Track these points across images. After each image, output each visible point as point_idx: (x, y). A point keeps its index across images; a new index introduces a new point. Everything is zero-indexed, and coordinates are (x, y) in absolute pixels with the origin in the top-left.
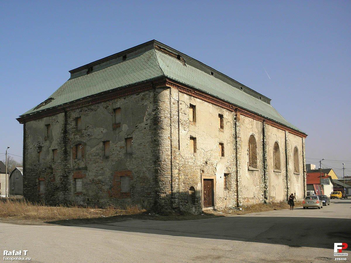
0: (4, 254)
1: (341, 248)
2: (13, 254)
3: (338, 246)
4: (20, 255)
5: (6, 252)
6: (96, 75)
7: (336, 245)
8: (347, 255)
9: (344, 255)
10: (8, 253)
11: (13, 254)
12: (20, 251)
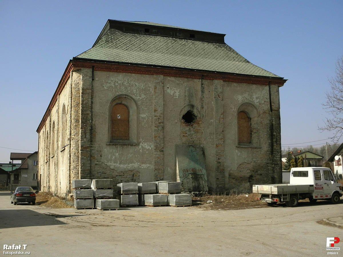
0: (4, 249)
1: (333, 242)
2: (13, 249)
3: (331, 241)
4: (20, 249)
5: (6, 246)
7: (328, 239)
8: (339, 249)
10: (7, 247)
11: (13, 249)
12: (20, 245)
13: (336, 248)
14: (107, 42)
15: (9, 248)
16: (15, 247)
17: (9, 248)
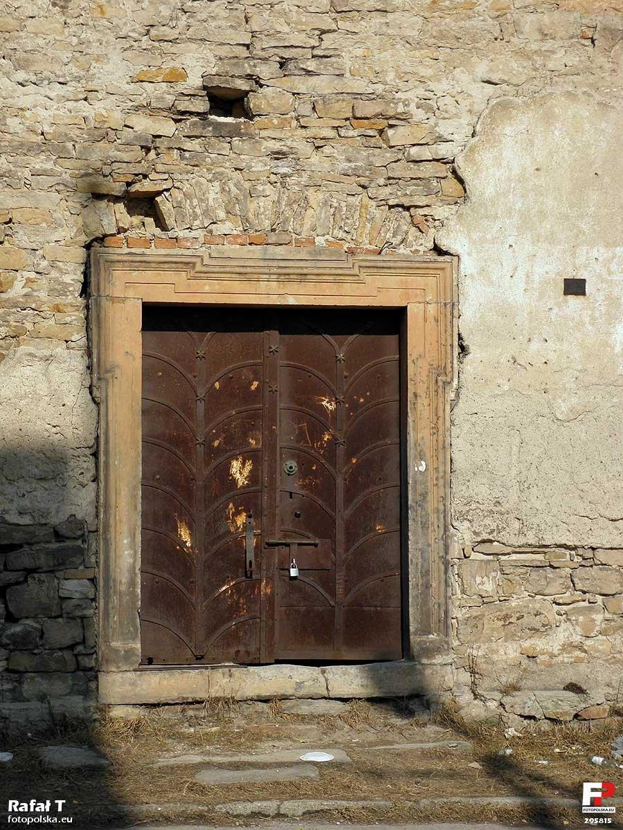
0: (10, 810)
1: (598, 794)
2: (32, 810)
3: (593, 790)
4: (48, 810)
5: (14, 804)
6: (418, 270)
8: (614, 812)
9: (606, 812)
10: (18, 807)
11: (32, 810)
12: (48, 802)
13: (605, 808)
14: (62, 728)
15: (21, 809)
16: (35, 807)
17: (37, 809)
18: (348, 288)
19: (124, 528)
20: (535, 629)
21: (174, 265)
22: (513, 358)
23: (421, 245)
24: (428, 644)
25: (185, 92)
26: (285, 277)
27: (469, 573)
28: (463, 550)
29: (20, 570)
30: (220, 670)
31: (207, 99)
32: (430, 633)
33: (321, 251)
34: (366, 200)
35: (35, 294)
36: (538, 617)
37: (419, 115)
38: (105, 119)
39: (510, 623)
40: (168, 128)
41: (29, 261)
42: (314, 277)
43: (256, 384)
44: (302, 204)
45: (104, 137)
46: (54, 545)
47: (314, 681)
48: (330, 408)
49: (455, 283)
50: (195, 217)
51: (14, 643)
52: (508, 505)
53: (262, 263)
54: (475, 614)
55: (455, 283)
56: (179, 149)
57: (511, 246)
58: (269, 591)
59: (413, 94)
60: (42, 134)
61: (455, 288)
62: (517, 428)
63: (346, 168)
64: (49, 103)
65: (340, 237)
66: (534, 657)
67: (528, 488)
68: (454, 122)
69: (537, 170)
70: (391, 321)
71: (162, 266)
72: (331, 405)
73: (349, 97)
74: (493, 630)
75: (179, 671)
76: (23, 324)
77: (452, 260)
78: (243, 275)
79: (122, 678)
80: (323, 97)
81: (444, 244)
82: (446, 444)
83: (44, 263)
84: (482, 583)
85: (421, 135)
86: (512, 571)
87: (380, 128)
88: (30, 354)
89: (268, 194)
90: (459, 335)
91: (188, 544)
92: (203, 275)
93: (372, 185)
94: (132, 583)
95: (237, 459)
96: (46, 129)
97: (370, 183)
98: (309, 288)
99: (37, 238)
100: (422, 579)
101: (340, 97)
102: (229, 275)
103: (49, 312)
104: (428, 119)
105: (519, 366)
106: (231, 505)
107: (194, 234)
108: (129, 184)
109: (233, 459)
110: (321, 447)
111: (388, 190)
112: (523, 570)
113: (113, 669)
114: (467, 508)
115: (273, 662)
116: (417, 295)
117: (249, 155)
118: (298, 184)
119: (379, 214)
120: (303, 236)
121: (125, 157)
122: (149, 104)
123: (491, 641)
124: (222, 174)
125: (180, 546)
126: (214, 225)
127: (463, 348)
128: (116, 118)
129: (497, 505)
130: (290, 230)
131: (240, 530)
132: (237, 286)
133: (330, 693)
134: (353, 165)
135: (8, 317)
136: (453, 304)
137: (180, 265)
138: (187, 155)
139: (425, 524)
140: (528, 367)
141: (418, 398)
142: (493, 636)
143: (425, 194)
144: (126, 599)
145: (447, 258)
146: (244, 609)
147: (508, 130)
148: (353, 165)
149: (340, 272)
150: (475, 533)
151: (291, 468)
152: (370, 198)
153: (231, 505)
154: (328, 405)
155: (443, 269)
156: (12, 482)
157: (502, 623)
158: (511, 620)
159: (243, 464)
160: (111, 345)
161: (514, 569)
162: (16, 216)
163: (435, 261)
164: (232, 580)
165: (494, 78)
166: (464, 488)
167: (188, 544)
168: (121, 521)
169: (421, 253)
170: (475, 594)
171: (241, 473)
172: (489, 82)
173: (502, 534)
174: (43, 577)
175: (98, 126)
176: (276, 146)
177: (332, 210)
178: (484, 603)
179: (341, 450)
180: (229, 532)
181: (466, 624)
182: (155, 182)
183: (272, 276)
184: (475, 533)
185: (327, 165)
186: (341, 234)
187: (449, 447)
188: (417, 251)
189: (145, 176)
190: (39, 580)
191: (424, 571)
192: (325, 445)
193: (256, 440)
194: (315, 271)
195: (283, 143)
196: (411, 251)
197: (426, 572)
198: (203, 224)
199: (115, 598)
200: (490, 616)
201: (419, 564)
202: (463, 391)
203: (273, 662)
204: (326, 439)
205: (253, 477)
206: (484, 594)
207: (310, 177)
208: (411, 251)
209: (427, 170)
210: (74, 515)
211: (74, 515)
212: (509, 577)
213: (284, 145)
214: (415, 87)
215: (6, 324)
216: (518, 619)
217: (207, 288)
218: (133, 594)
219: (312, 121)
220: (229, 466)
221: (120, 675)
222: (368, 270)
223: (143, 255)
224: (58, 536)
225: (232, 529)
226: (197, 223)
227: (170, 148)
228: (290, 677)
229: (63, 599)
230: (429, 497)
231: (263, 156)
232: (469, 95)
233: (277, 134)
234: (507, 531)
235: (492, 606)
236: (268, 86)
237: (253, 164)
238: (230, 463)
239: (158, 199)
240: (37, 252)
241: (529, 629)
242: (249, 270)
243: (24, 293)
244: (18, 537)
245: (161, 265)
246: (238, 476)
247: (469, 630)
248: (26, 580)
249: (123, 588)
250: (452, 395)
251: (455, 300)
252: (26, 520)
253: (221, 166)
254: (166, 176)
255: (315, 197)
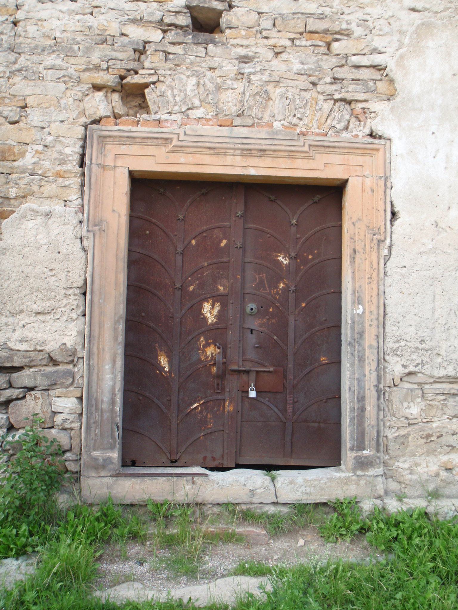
18: (299, 163)
19: (107, 356)
20: (452, 446)
21: (155, 141)
22: (436, 222)
23: (360, 131)
24: (363, 459)
25: (171, 9)
26: (247, 153)
27: (398, 399)
28: (393, 380)
29: (21, 388)
30: (185, 478)
31: (189, 15)
32: (364, 449)
33: (277, 132)
34: (315, 95)
35: (42, 162)
36: (455, 436)
37: (358, 31)
38: (106, 28)
39: (431, 441)
40: (156, 35)
41: (38, 136)
42: (272, 153)
43: (224, 242)
44: (263, 95)
45: (104, 41)
46: (50, 369)
47: (265, 488)
48: (285, 262)
49: (388, 161)
50: (175, 104)
51: (14, 448)
52: (431, 343)
53: (228, 140)
54: (403, 433)
55: (388, 161)
56: (164, 52)
57: (433, 133)
58: (231, 409)
59: (355, 17)
60: (55, 39)
61: (388, 165)
62: (439, 279)
63: (300, 68)
64: (61, 16)
65: (293, 122)
66: (450, 469)
67: (448, 329)
68: (387, 39)
69: (454, 75)
70: (333, 192)
71: (146, 141)
72: (286, 260)
73: (303, 16)
74: (417, 446)
75: (150, 478)
76: (31, 186)
77: (386, 143)
78: (212, 150)
79: (101, 481)
80: (282, 15)
81: (379, 129)
82: (380, 291)
83: (50, 138)
84: (409, 407)
85: (361, 46)
86: (433, 397)
87: (328, 40)
88: (33, 210)
89: (236, 87)
90: (391, 202)
91: (167, 369)
92: (179, 149)
93: (321, 82)
94: (113, 402)
95: (208, 302)
96: (58, 35)
97: (319, 81)
98: (268, 162)
99: (46, 118)
100: (358, 403)
101: (296, 16)
102: (200, 150)
103: (52, 178)
104: (366, 35)
105: (440, 229)
106: (202, 339)
107: (173, 117)
108: (122, 78)
109: (205, 301)
110: (277, 293)
111: (334, 87)
112: (443, 397)
113: (93, 474)
114: (397, 345)
115: (234, 466)
116: (356, 171)
117: (220, 55)
118: (260, 80)
119: (327, 106)
120: (263, 121)
121: (120, 56)
122: (142, 19)
123: (415, 455)
124: (196, 71)
125: (160, 371)
126: (191, 111)
127: (394, 214)
128: (114, 28)
129: (422, 343)
130: (253, 115)
131: (209, 359)
132: (207, 159)
133: (278, 499)
134: (306, 67)
135: (19, 181)
136: (387, 178)
137: (160, 141)
138: (171, 56)
139: (362, 357)
140: (448, 229)
141: (357, 253)
142: (417, 452)
143: (364, 91)
144: (106, 415)
145: (382, 141)
146: (211, 423)
147: (430, 43)
148: (306, 67)
149: (293, 148)
150: (403, 366)
151: (252, 309)
152: (319, 93)
153: (202, 339)
154: (283, 260)
155: (378, 150)
156: (15, 315)
157: (425, 440)
158: (432, 439)
159: (213, 306)
160: (100, 205)
161: (435, 396)
162: (30, 101)
163: (372, 143)
164: (202, 399)
165: (419, 6)
166: (395, 328)
167: (167, 369)
168: (103, 350)
169: (360, 137)
170: (402, 417)
171: (211, 313)
172: (413, 10)
173: (426, 367)
174: (38, 394)
175: (101, 33)
176: (242, 52)
177: (288, 101)
178: (409, 424)
179: (292, 296)
180: (200, 361)
181: (395, 442)
182: (143, 76)
183: (237, 151)
184: (403, 366)
185: (283, 67)
186: (295, 121)
187: (383, 294)
188: (357, 136)
189: (136, 73)
190: (35, 397)
191: (360, 398)
192: (280, 292)
193: (223, 287)
194: (273, 148)
195: (249, 50)
196: (352, 136)
197: (362, 398)
198: (181, 109)
199: (97, 414)
200: (415, 435)
201: (356, 391)
202: (394, 248)
203: (234, 466)
204: (281, 287)
205: (220, 316)
206: (410, 417)
207: (270, 75)
208: (352, 136)
209: (364, 74)
210: (65, 344)
211: (65, 344)
212: (431, 403)
213: (250, 51)
214: (356, 11)
215: (17, 186)
216: (438, 437)
217: (182, 160)
218: (112, 411)
219: (273, 33)
220: (201, 307)
221: (99, 479)
222: (317, 149)
223: (130, 131)
224: (53, 361)
225: (203, 358)
226: (176, 108)
227: (156, 51)
228: (245, 485)
229: (55, 413)
230: (366, 335)
231: (232, 59)
232: (399, 19)
233: (245, 42)
234: (431, 364)
235: (416, 427)
236: (238, 7)
237: (224, 65)
238: (202, 305)
239: (146, 91)
240: (45, 130)
241: (447, 446)
242: (217, 145)
243: (32, 162)
244: (17, 362)
245: (145, 140)
246: (208, 315)
247: (397, 447)
248: (24, 397)
249: (105, 406)
250: (386, 252)
251: (388, 174)
252: (23, 347)
253: (198, 66)
254: (152, 72)
255: (276, 92)
